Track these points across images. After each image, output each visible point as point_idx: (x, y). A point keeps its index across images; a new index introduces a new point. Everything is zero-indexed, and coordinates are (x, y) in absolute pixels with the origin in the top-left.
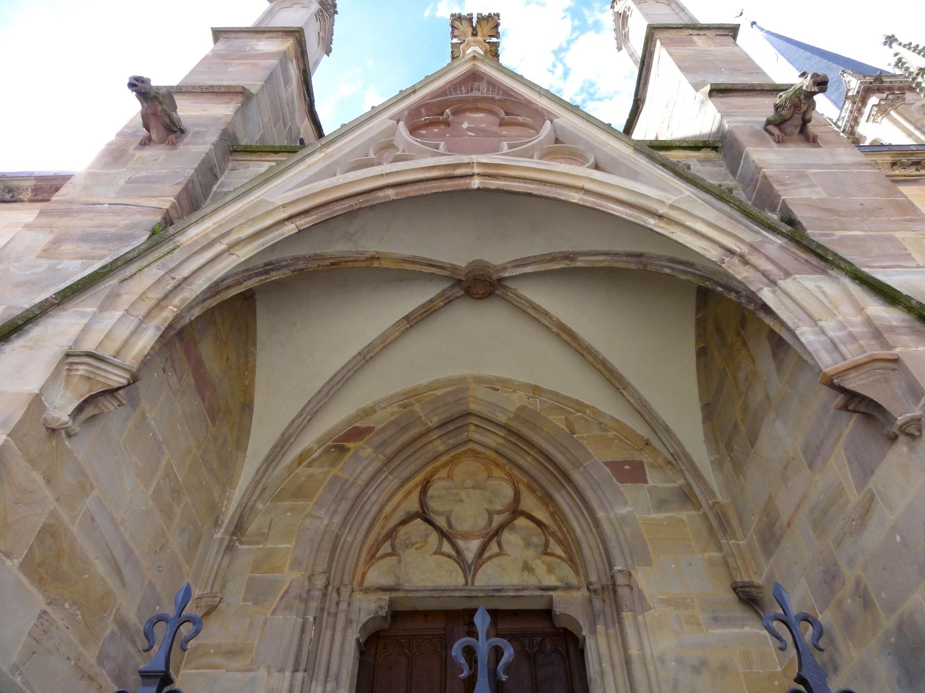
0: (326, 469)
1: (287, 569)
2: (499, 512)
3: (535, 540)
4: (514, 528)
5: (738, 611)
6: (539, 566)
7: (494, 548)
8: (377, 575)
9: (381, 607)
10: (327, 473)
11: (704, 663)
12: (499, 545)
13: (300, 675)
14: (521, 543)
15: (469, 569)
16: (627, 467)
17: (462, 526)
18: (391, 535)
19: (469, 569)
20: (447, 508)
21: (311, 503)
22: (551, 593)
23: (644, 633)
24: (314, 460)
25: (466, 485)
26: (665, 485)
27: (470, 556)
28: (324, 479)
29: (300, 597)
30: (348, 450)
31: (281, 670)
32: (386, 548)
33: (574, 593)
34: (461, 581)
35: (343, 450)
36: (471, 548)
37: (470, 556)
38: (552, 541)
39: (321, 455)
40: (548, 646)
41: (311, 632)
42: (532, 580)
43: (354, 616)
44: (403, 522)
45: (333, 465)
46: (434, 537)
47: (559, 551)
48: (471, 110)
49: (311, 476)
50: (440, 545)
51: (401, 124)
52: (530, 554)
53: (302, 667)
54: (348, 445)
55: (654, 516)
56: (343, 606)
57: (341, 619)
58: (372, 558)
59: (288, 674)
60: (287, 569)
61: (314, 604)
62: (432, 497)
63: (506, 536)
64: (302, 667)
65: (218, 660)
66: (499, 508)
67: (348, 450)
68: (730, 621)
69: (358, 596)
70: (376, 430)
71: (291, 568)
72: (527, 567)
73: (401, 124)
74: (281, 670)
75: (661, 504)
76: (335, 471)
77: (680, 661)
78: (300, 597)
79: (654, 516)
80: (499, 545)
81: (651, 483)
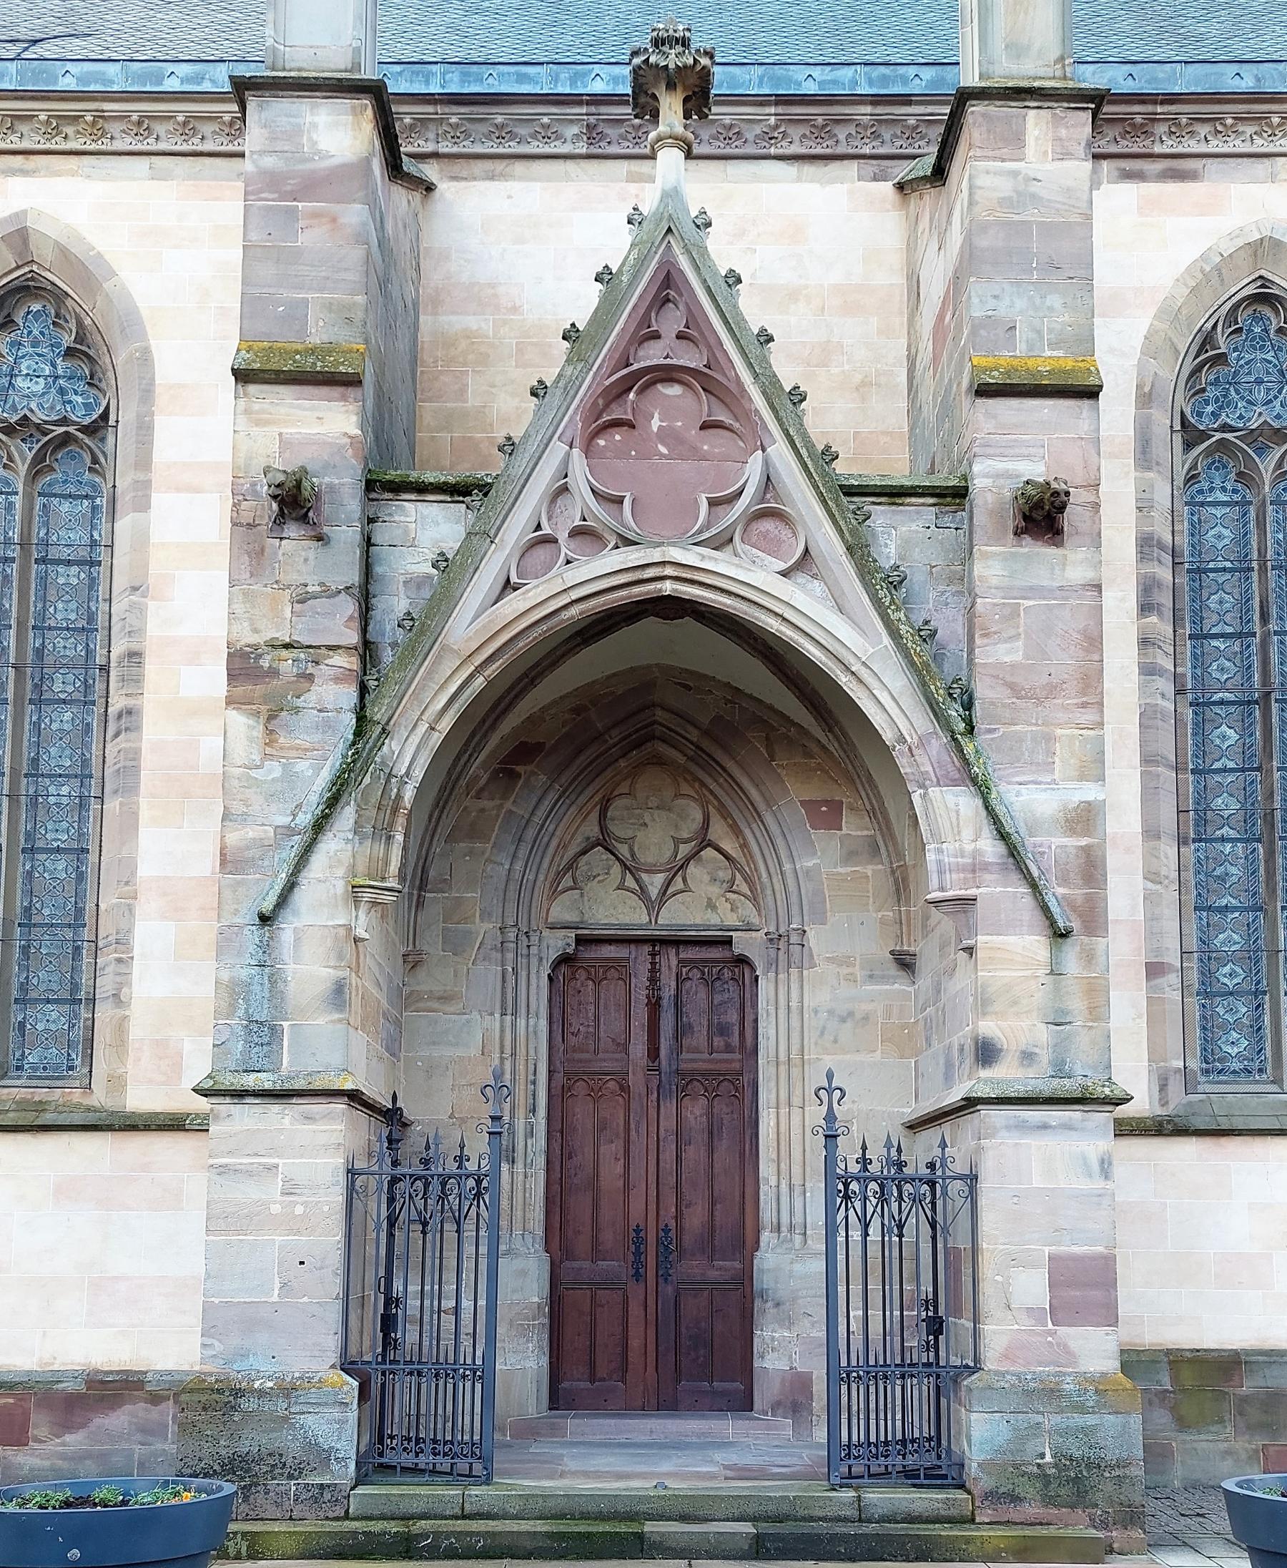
0: (498, 802)
1: (477, 920)
2: (686, 841)
3: (721, 874)
4: (700, 859)
5: (893, 970)
6: (723, 906)
7: (678, 883)
8: (561, 910)
9: (568, 945)
10: (501, 806)
11: (851, 1014)
12: (684, 880)
13: (508, 1018)
14: (706, 878)
15: (654, 906)
16: (824, 809)
17: (647, 857)
18: (571, 866)
19: (654, 906)
20: (630, 834)
21: (489, 846)
22: (731, 933)
23: (806, 987)
24: (482, 789)
25: (650, 805)
26: (859, 833)
27: (654, 892)
28: (498, 816)
29: (494, 948)
30: (519, 776)
31: (492, 1014)
32: (567, 881)
33: (754, 934)
34: (645, 919)
35: (513, 776)
36: (655, 883)
37: (654, 892)
38: (738, 876)
39: (487, 783)
40: (727, 974)
41: (511, 979)
42: (714, 919)
43: (544, 955)
44: (584, 852)
45: (505, 797)
46: (617, 869)
47: (745, 889)
48: (662, 381)
49: (483, 810)
50: (623, 879)
51: (575, 451)
52: (715, 890)
53: (509, 1011)
54: (520, 769)
55: (840, 870)
56: (534, 950)
57: (534, 961)
58: (554, 893)
59: (497, 1016)
60: (477, 920)
61: (510, 956)
62: (613, 819)
63: (692, 869)
64: (509, 1011)
65: (436, 1005)
66: (685, 835)
67: (519, 776)
68: (884, 979)
69: (546, 933)
70: (547, 746)
71: (482, 920)
72: (711, 906)
73: (575, 451)
74: (492, 1014)
75: (850, 856)
76: (508, 805)
77: (831, 1012)
78: (494, 948)
79: (840, 870)
80: (684, 880)
81: (845, 831)
